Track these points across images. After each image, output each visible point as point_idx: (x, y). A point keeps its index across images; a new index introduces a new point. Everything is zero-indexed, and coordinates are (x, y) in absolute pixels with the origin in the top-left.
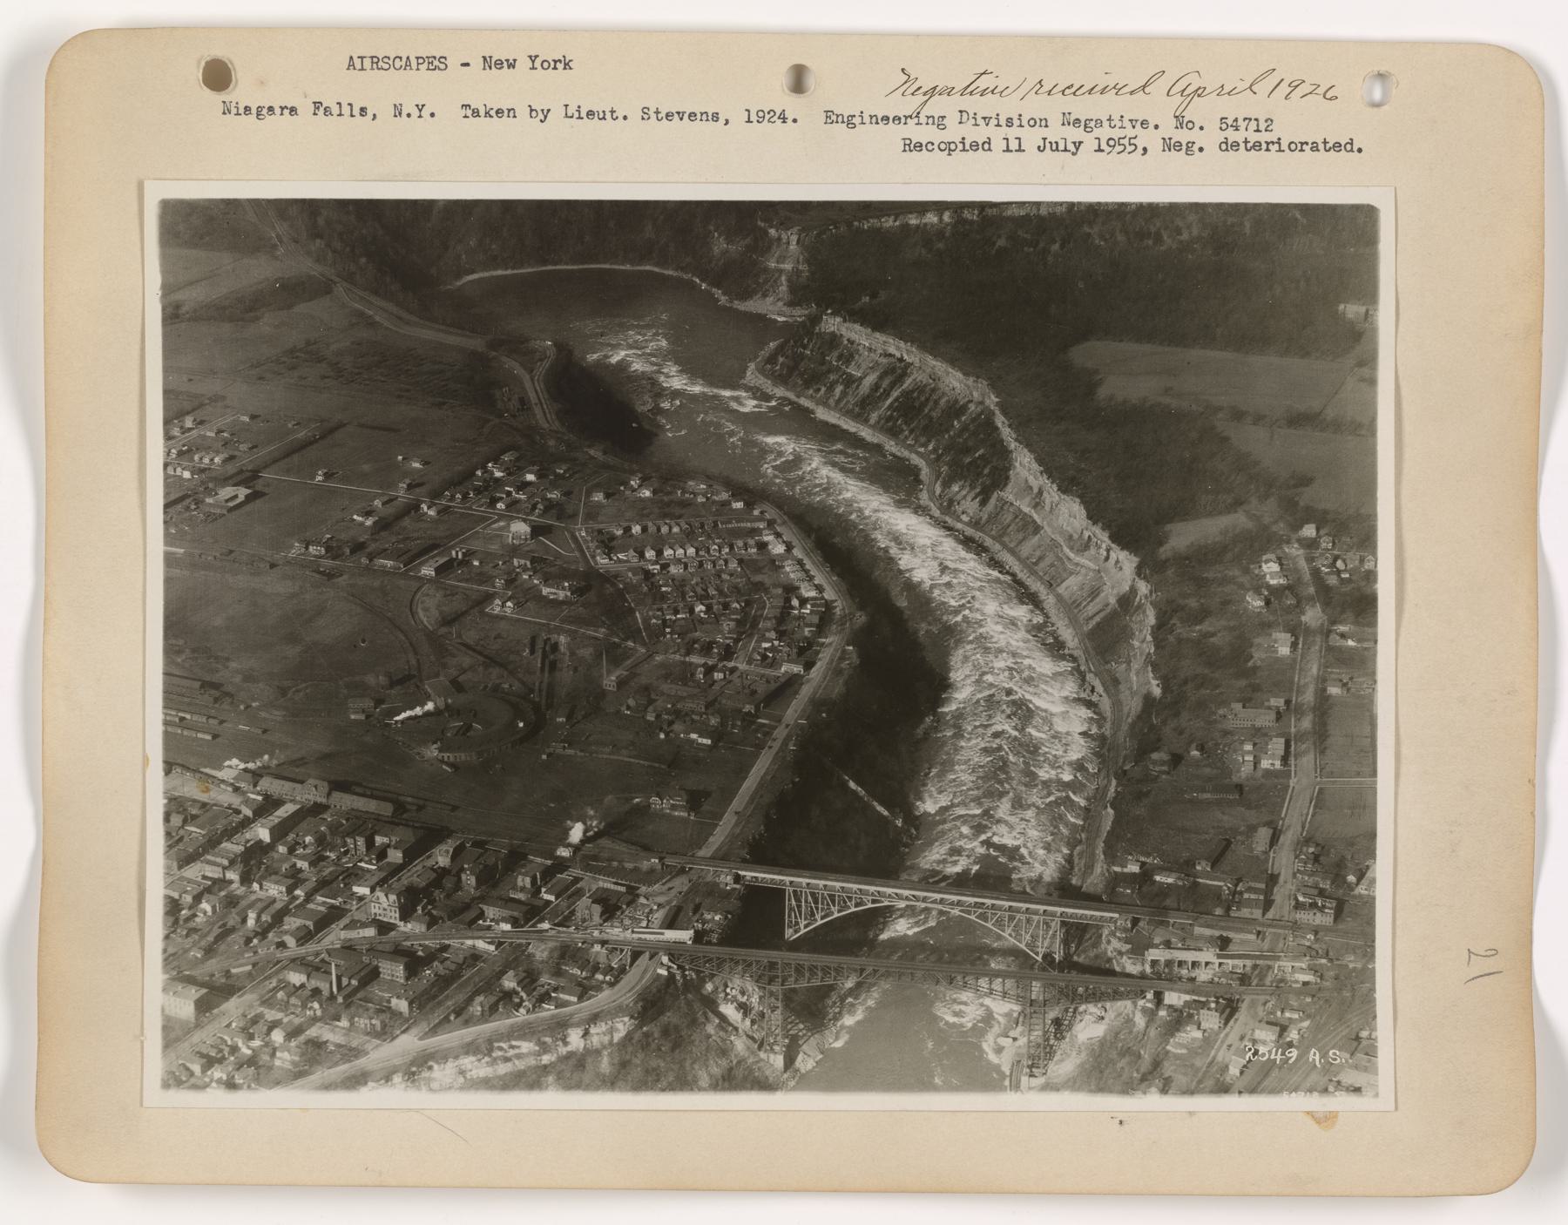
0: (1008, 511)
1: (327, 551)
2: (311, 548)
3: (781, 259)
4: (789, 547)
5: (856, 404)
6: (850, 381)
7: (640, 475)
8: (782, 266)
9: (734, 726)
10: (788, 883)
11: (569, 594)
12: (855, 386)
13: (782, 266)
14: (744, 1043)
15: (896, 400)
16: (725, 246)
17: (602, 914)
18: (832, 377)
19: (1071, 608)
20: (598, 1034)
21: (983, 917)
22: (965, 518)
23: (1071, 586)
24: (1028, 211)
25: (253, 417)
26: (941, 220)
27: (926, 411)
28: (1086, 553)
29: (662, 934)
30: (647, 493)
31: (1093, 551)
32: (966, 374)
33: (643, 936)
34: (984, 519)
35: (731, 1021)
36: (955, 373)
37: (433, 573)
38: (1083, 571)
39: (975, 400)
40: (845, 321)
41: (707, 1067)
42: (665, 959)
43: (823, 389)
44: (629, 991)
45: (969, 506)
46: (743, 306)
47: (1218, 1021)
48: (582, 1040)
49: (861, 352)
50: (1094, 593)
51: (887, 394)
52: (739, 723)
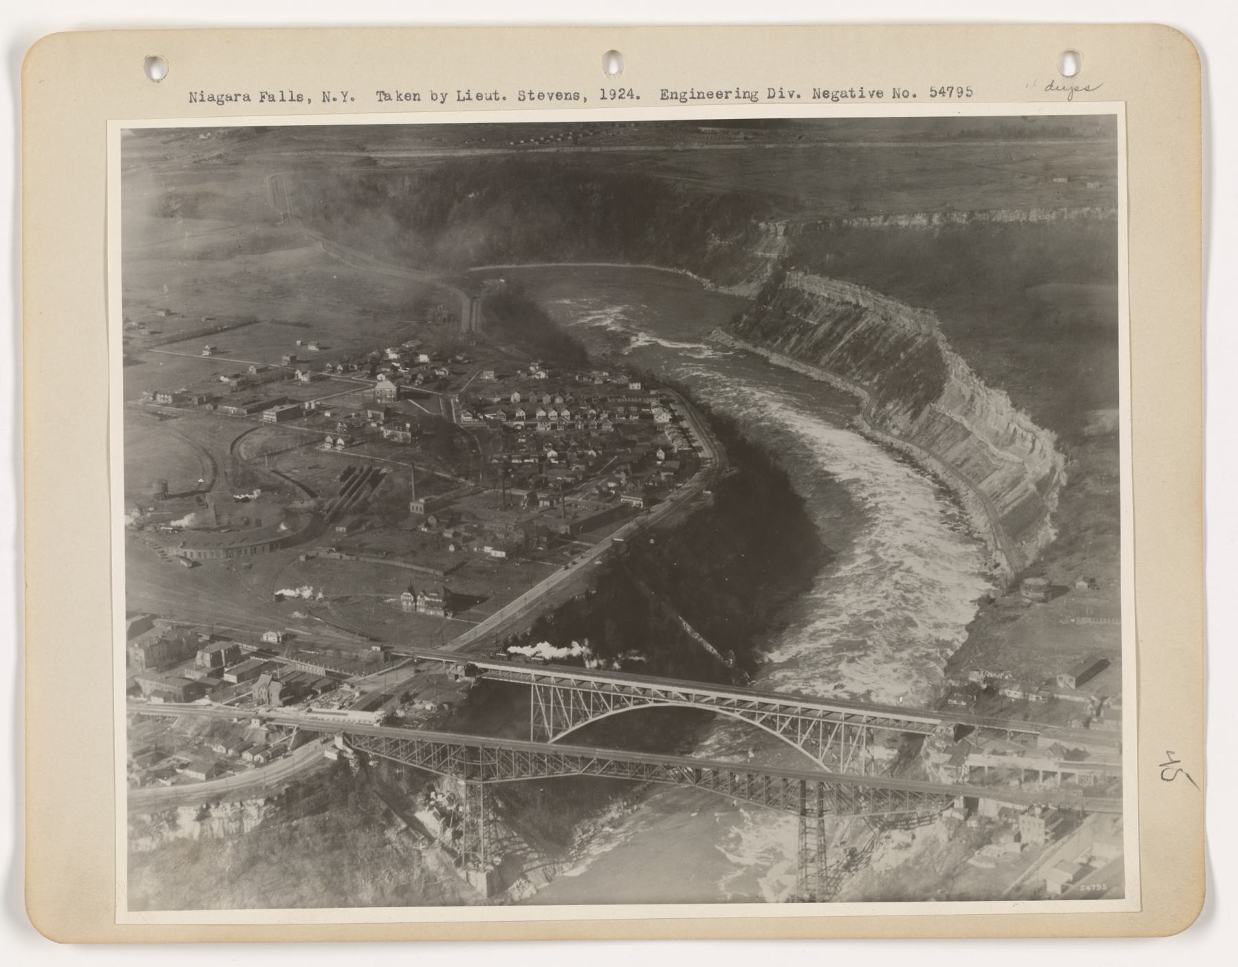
0: (940, 421)
1: (174, 401)
2: (158, 397)
3: (769, 248)
4: (675, 420)
5: (809, 349)
6: (806, 329)
7: (540, 361)
8: (768, 255)
9: (539, 543)
10: (533, 678)
11: (409, 434)
12: (810, 333)
13: (768, 255)
14: (437, 856)
15: (849, 341)
16: (718, 241)
17: (282, 695)
18: (790, 327)
19: (988, 500)
20: (220, 818)
21: (769, 722)
22: (896, 432)
23: (993, 482)
24: (1018, 218)
25: (168, 313)
26: (930, 221)
27: (875, 348)
28: (1011, 447)
29: (346, 715)
30: (543, 375)
31: (1018, 443)
32: (914, 306)
33: (320, 716)
34: (914, 431)
35: (426, 830)
36: (904, 308)
37: (275, 418)
38: (1007, 466)
39: (923, 332)
40: (806, 274)
41: (375, 876)
42: (339, 742)
43: (780, 339)
44: (277, 773)
45: (901, 420)
46: (723, 290)
47: (1042, 830)
48: (198, 824)
49: (820, 303)
50: (1015, 482)
51: (840, 337)
52: (545, 539)
